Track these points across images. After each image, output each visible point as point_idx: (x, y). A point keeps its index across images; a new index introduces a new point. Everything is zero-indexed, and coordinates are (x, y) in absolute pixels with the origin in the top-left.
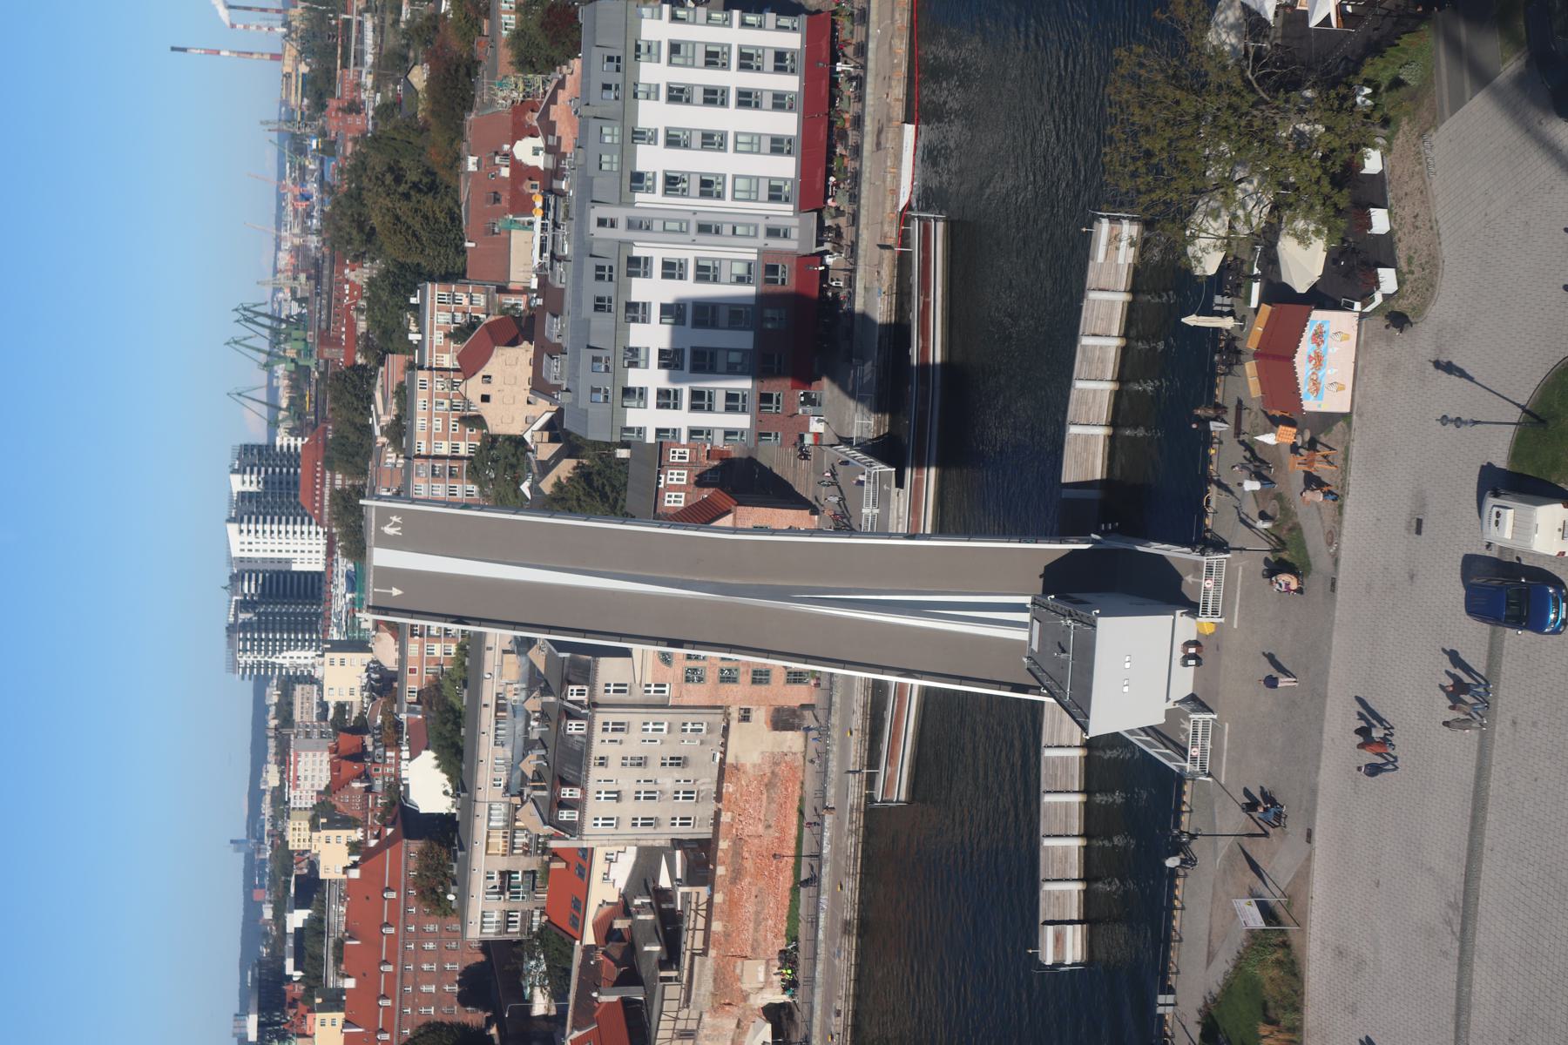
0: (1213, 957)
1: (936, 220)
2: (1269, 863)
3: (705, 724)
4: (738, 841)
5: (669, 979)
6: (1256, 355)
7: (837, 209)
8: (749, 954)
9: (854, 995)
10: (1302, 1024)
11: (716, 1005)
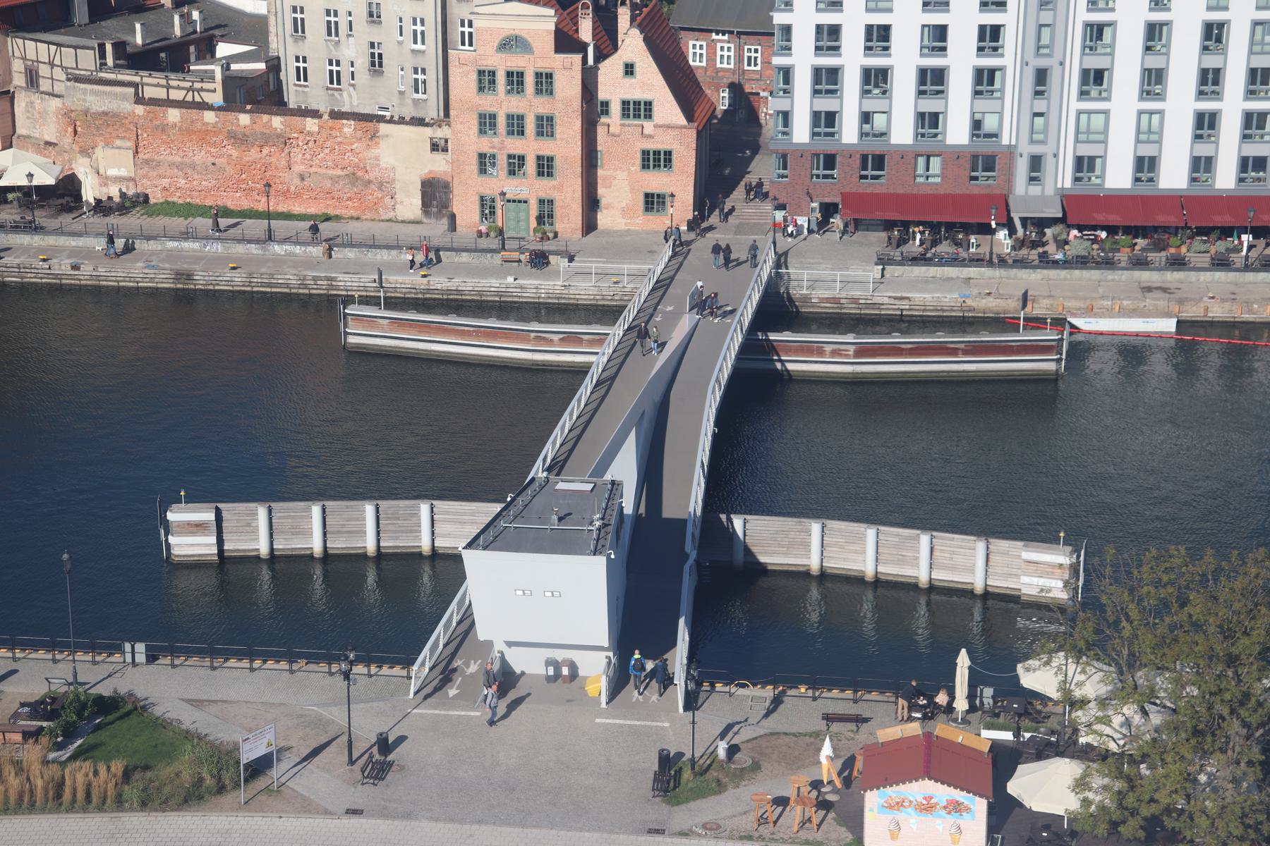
2: (318, 767)
3: (425, 97)
4: (285, 141)
5: (103, 55)
6: (928, 736)
7: (1066, 242)
8: (140, 155)
9: (100, 287)
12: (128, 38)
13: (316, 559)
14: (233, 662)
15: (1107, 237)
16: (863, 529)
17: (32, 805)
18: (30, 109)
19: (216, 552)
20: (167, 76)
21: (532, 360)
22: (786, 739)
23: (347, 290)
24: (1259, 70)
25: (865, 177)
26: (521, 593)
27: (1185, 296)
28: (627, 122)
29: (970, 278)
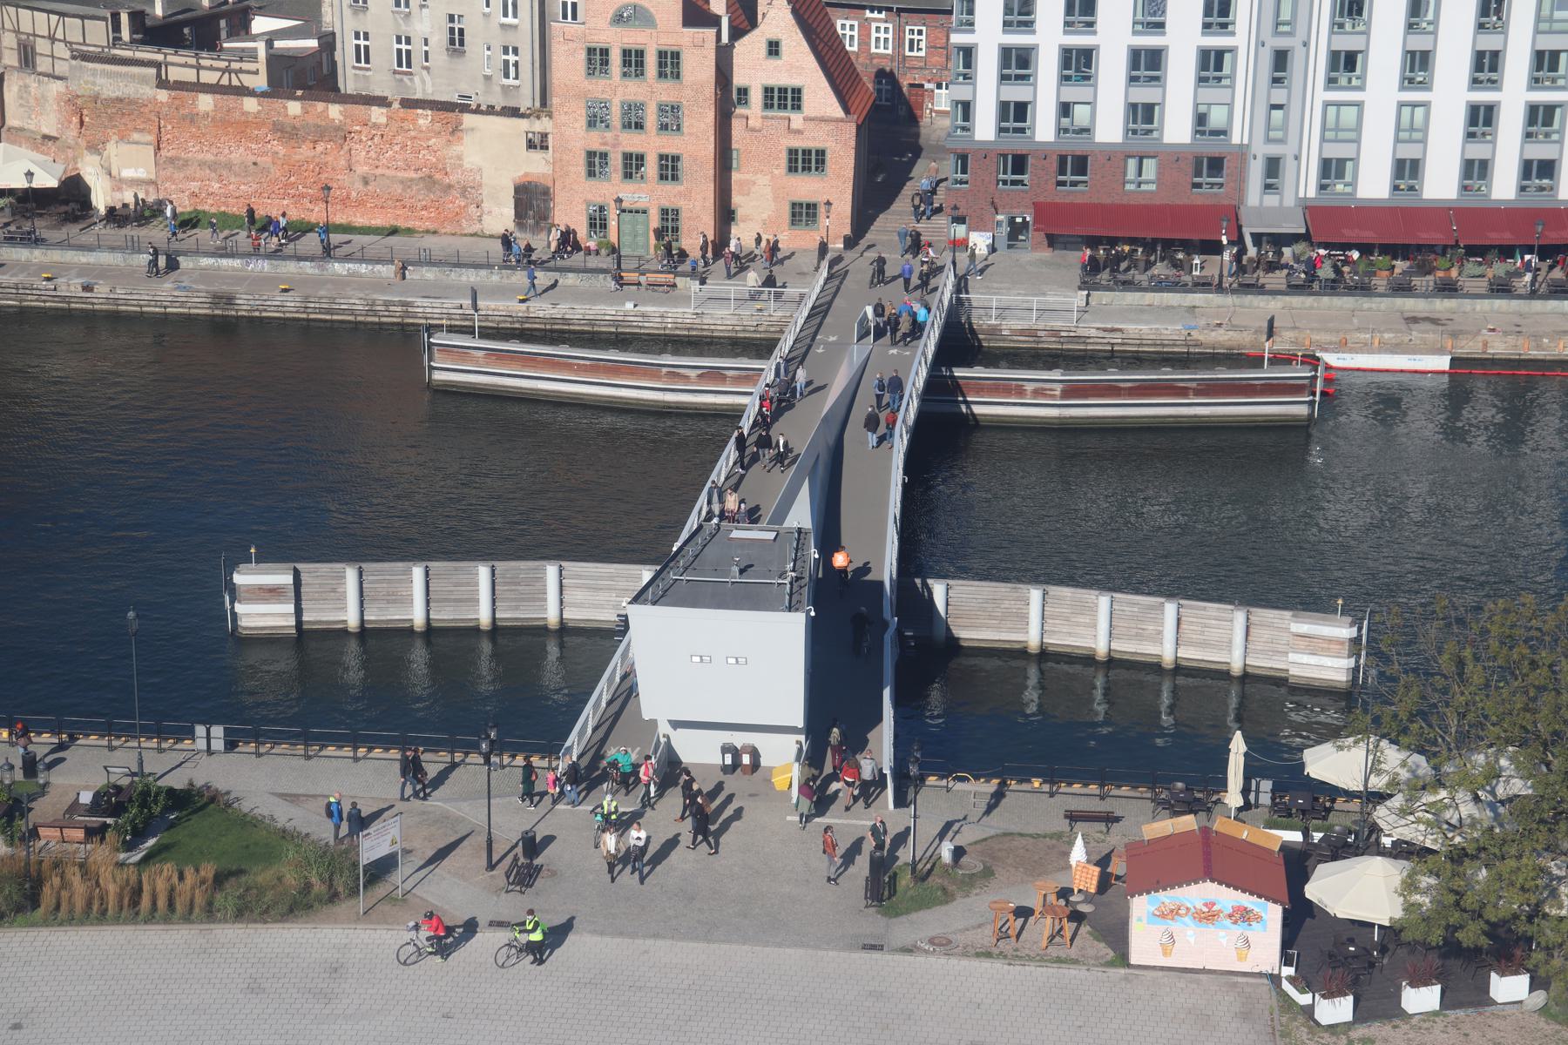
0: (292, 802)
1: (1312, 403)
2: (449, 872)
3: (517, 83)
4: (342, 135)
5: (117, 28)
6: (1205, 831)
8: (163, 153)
10: (220, 921)
11: (79, 102)
12: (148, 10)
13: (417, 632)
14: (330, 750)
15: (1361, 257)
16: (1094, 597)
17: (104, 912)
18: (25, 95)
19: (294, 623)
20: (197, 54)
21: (664, 402)
22: (1023, 841)
23: (426, 318)
24: (1547, 53)
25: (1063, 183)
26: (698, 659)
27: (1460, 328)
28: (770, 113)
29: (1194, 307)
